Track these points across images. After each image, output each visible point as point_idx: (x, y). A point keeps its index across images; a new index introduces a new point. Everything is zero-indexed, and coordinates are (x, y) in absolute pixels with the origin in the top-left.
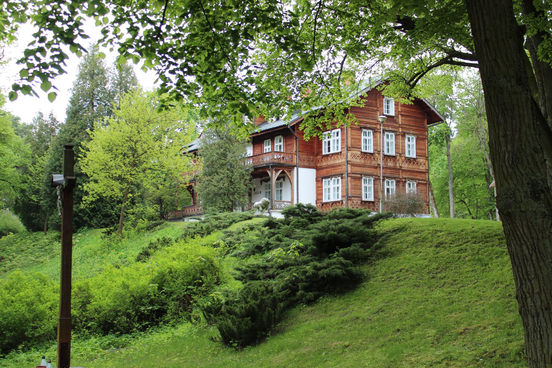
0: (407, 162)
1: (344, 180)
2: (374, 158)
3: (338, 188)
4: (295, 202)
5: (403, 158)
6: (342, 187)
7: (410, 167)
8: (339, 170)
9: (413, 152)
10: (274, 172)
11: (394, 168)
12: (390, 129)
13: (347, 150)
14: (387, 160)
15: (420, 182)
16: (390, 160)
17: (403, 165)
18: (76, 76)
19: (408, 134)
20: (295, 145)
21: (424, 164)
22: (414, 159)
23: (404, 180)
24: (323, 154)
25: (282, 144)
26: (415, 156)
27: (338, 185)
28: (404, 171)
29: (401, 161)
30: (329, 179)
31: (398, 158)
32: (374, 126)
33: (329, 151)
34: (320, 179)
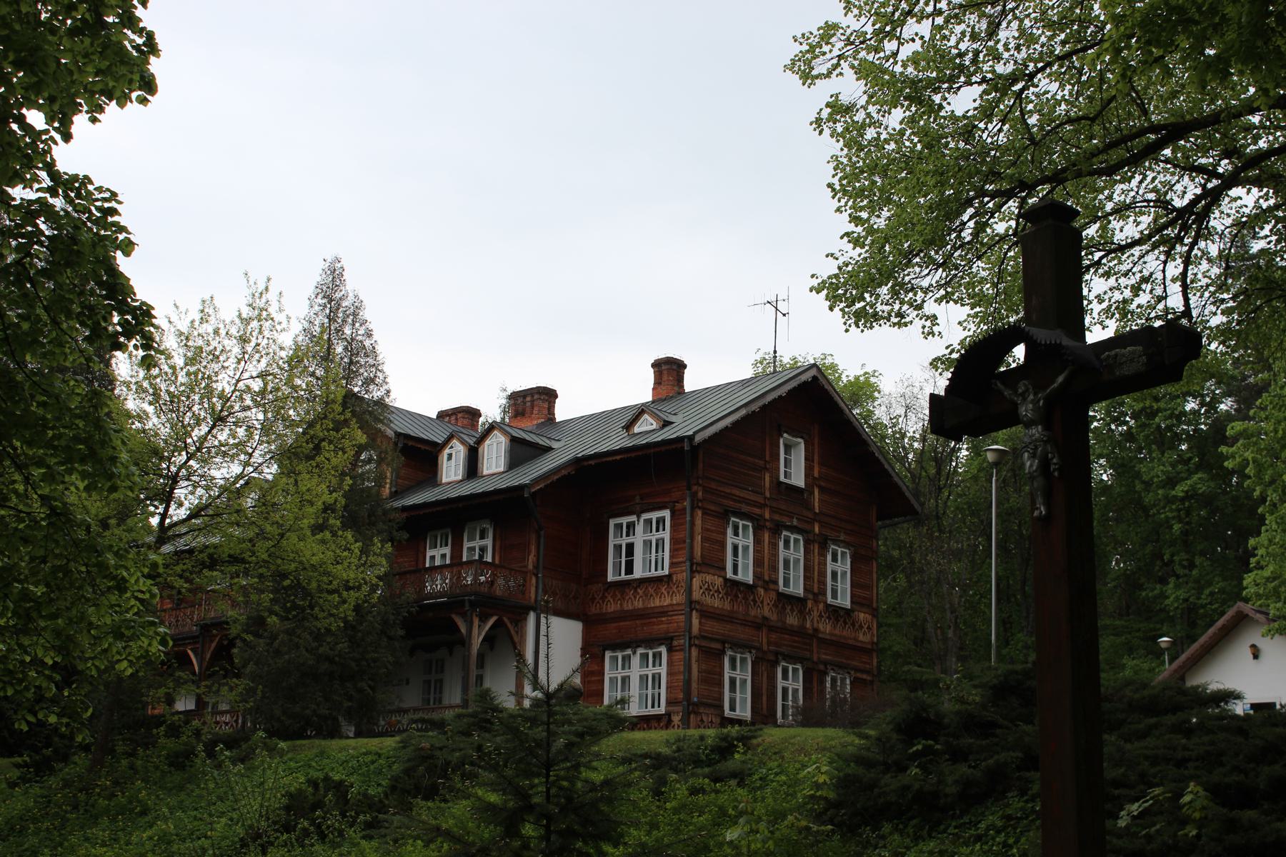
0: (829, 618)
1: (678, 656)
2: (754, 601)
5: (821, 606)
6: (669, 674)
7: (837, 632)
8: (661, 627)
9: (844, 591)
10: (476, 622)
11: (799, 632)
12: (795, 522)
13: (692, 572)
14: (784, 608)
15: (859, 675)
16: (792, 610)
17: (821, 627)
18: (669, 372)
19: (836, 542)
20: (533, 548)
21: (869, 628)
22: (848, 612)
23: (822, 667)
24: (611, 577)
25: (488, 542)
26: (847, 603)
27: (657, 670)
28: (823, 642)
29: (816, 613)
30: (629, 652)
31: (810, 604)
32: (757, 511)
33: (630, 570)
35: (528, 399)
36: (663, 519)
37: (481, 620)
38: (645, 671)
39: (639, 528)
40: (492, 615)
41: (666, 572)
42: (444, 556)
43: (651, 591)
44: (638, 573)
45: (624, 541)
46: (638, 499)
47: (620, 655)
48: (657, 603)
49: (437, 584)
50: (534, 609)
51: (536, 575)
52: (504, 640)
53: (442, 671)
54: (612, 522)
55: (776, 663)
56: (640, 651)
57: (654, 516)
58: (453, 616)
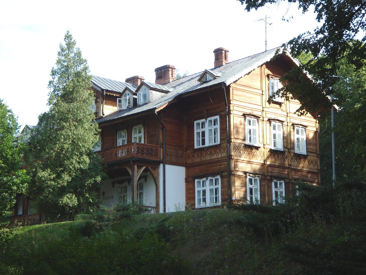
0: (296, 159)
1: (225, 180)
3: (216, 190)
4: (161, 211)
5: (292, 154)
6: (222, 187)
24: (196, 147)
25: (142, 134)
30: (205, 179)
31: (286, 154)
33: (203, 143)
34: (191, 179)
35: (163, 70)
36: (217, 119)
37: (138, 168)
38: (211, 187)
39: (207, 124)
40: (143, 166)
41: (219, 143)
42: (124, 141)
43: (213, 152)
44: (207, 144)
45: (200, 131)
46: (205, 112)
47: (201, 181)
48: (216, 157)
49: (121, 154)
50: (162, 163)
51: (163, 148)
52: (150, 175)
53: (142, 189)
54: (196, 122)
55: (271, 180)
56: (209, 178)
57: (212, 118)
58: (126, 167)
